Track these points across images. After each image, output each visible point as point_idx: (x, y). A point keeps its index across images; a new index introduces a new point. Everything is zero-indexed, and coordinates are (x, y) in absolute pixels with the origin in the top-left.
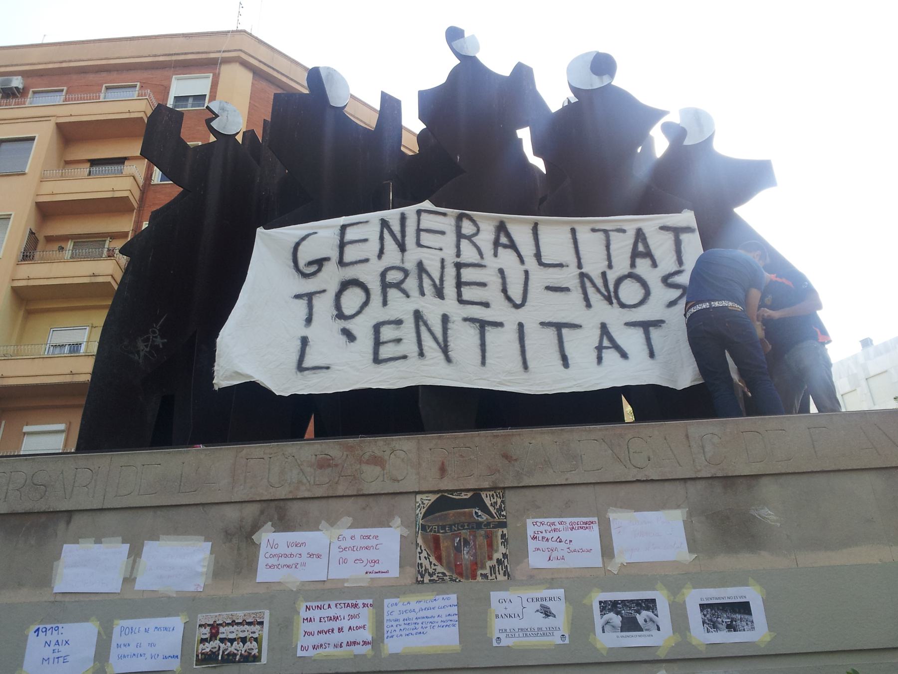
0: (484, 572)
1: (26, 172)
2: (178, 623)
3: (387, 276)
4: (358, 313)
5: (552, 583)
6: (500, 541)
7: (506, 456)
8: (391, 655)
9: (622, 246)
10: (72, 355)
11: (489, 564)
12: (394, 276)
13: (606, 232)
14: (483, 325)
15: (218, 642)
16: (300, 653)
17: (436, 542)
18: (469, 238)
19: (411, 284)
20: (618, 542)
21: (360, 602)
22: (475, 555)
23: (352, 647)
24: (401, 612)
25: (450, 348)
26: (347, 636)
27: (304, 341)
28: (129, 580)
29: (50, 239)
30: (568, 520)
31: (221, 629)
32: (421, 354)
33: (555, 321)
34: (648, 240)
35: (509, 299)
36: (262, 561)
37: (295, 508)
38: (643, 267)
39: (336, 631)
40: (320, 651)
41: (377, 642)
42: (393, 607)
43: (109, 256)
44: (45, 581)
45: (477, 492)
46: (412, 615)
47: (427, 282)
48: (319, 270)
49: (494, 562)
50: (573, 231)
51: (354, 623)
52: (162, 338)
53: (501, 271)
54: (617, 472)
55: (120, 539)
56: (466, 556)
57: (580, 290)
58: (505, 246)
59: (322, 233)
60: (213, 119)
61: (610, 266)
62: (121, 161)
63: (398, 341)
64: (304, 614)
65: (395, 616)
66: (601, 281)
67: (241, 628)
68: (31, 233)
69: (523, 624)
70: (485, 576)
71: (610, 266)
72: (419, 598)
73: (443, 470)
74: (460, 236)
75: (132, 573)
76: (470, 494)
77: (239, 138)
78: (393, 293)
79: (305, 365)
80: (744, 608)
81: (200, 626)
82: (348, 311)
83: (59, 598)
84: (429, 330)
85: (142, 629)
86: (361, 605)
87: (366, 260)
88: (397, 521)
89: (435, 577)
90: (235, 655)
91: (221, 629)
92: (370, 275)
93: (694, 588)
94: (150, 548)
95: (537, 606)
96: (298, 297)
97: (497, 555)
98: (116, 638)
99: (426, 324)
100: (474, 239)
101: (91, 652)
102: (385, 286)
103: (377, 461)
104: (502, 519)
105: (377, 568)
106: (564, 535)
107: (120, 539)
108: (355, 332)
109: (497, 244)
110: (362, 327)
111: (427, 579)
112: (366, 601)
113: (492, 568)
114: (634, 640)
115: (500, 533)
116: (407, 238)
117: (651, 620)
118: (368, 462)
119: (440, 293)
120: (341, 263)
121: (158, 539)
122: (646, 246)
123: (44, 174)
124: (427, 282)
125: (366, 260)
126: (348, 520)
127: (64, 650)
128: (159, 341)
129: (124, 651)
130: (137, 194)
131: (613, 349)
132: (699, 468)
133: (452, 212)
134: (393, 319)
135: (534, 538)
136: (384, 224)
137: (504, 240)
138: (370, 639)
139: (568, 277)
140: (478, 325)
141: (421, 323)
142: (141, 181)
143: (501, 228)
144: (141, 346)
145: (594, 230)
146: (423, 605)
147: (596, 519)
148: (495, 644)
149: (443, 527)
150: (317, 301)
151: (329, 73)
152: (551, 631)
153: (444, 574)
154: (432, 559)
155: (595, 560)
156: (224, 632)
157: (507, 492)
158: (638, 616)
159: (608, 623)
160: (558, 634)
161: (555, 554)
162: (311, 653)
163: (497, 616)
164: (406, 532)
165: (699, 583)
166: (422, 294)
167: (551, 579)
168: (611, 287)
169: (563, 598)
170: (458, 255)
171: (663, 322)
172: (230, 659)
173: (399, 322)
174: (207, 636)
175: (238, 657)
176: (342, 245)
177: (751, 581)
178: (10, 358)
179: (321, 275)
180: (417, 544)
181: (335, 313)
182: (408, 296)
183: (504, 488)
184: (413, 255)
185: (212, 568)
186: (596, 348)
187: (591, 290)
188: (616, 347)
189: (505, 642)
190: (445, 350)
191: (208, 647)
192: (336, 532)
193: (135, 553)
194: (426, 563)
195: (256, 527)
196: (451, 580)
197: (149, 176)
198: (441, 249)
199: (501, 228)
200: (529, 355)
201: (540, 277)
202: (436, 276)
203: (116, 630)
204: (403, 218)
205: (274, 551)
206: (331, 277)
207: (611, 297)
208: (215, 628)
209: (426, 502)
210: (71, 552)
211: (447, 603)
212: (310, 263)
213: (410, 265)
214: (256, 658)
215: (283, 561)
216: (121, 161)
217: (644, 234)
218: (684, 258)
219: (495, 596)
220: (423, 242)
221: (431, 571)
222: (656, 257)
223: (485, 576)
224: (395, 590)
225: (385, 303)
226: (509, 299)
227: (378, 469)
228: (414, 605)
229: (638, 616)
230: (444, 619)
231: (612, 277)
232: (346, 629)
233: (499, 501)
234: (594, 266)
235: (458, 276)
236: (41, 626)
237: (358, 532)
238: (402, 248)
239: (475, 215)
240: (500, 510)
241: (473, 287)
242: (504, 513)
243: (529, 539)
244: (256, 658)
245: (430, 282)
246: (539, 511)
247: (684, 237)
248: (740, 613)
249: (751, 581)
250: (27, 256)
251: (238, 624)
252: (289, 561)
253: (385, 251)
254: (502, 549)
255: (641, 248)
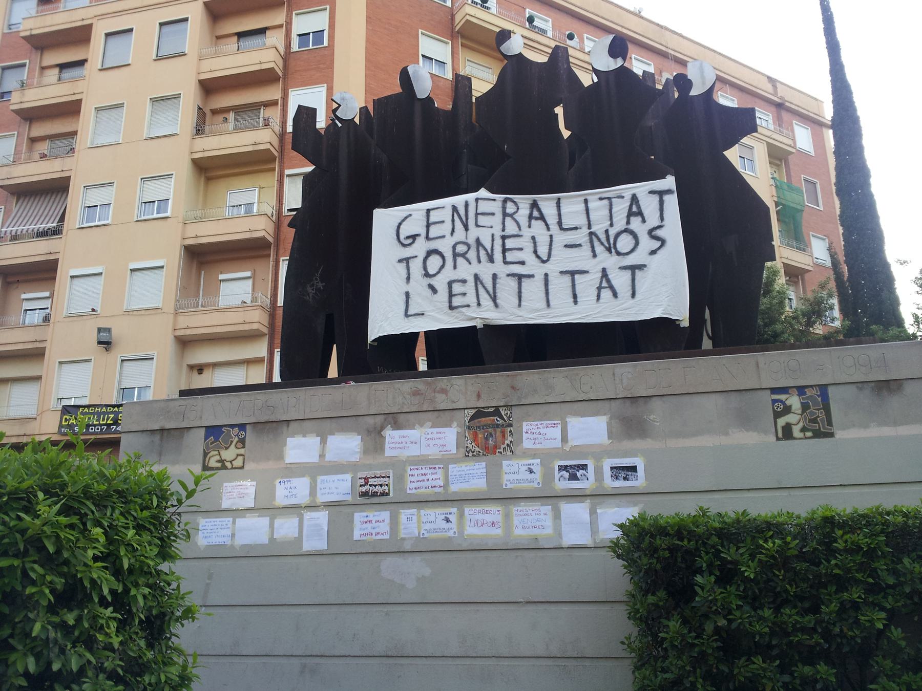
0: (499, 450)
1: (186, 52)
2: (348, 477)
3: (457, 248)
4: (438, 272)
5: (534, 456)
6: (509, 434)
7: (513, 388)
8: (453, 492)
9: (621, 208)
10: (249, 215)
11: (503, 446)
12: (461, 249)
13: (609, 199)
14: (520, 277)
15: (368, 486)
16: (408, 492)
17: (476, 435)
18: (511, 215)
19: (472, 255)
20: (571, 433)
21: (437, 466)
22: (496, 442)
23: (434, 489)
24: (458, 471)
25: (497, 298)
26: (430, 483)
27: (407, 295)
28: (322, 456)
29: (215, 112)
30: (545, 423)
31: (370, 480)
32: (479, 304)
33: (570, 269)
34: (640, 202)
35: (538, 257)
36: (387, 445)
37: (402, 418)
38: (636, 223)
39: (426, 480)
40: (418, 490)
41: (446, 486)
42: (454, 469)
43: (266, 125)
44: (280, 457)
45: (497, 408)
46: (462, 473)
47: (482, 253)
48: (413, 242)
49: (505, 445)
50: (586, 201)
51: (434, 477)
52: (322, 283)
53: (533, 238)
54: (573, 396)
55: (315, 434)
56: (491, 442)
57: (589, 244)
58: (537, 219)
59: (416, 215)
60: (337, 109)
61: (611, 225)
62: (262, 31)
63: (464, 294)
64: (409, 472)
65: (455, 473)
66: (605, 236)
67: (379, 479)
68: (200, 109)
69: (519, 477)
70: (501, 453)
71: (611, 225)
72: (467, 464)
73: (479, 396)
74: (505, 215)
75: (323, 452)
76: (493, 409)
77: (357, 120)
78: (460, 260)
79: (409, 313)
80: (634, 469)
81: (360, 478)
82: (431, 271)
83: (288, 466)
84: (484, 287)
85: (331, 480)
86: (437, 468)
87: (444, 237)
88: (455, 424)
89: (475, 453)
90: (377, 492)
91: (370, 480)
92: (445, 246)
93: (609, 458)
94: (331, 439)
95: (443, 517)
96: (400, 261)
97: (507, 442)
98: (319, 485)
99: (482, 283)
100: (515, 216)
101: (307, 492)
102: (455, 255)
103: (444, 391)
104: (510, 422)
105: (445, 449)
106: (543, 431)
107: (315, 434)
108: (436, 287)
109: (531, 217)
110: (440, 282)
111: (471, 454)
112: (440, 466)
113: (504, 449)
114: (575, 485)
115: (509, 430)
116: (469, 220)
117: (585, 475)
118: (439, 392)
119: (491, 259)
120: (427, 238)
121: (334, 435)
122: (639, 207)
123: (201, 53)
124: (482, 253)
125: (444, 237)
126: (429, 424)
127: (295, 492)
128: (320, 285)
129: (324, 491)
130: (280, 63)
131: (608, 289)
132: (618, 392)
133: (500, 197)
134: (460, 279)
135: (526, 433)
136: (455, 209)
137: (536, 214)
138: (442, 485)
139: (581, 236)
140: (517, 278)
141: (478, 283)
142: (282, 51)
143: (534, 205)
144: (309, 290)
145: (601, 199)
146: (468, 468)
147: (560, 422)
148: (504, 487)
149: (479, 427)
150: (412, 264)
151: (415, 70)
152: (533, 480)
153: (479, 452)
154: (473, 444)
155: (558, 444)
156: (371, 481)
157: (513, 407)
158: (577, 473)
159: (562, 476)
160: (536, 482)
161: (537, 441)
162: (414, 491)
163: (506, 473)
164: (459, 430)
165: (611, 455)
166: (479, 262)
167: (534, 454)
168: (612, 241)
169: (539, 464)
170: (503, 230)
171: (645, 266)
172: (375, 494)
173: (464, 281)
174: (363, 483)
175: (379, 494)
176: (428, 226)
177: (639, 455)
178: (200, 220)
179: (414, 245)
180: (466, 436)
181: (424, 272)
182: (470, 263)
183: (512, 406)
184: (474, 232)
185: (363, 448)
186: (597, 288)
187: (596, 243)
188: (611, 287)
189: (509, 486)
190: (494, 299)
191: (364, 489)
192: (424, 430)
193: (324, 442)
194: (470, 446)
195: (382, 428)
196: (483, 455)
197: (289, 43)
198: (492, 227)
199: (534, 205)
200: (550, 297)
201: (561, 238)
202: (489, 247)
203: (319, 481)
204: (467, 205)
205: (393, 441)
206: (420, 248)
207: (611, 248)
208: (366, 479)
209: (470, 413)
210: (292, 442)
211: (481, 467)
212: (408, 237)
213: (471, 241)
214: (388, 494)
215: (397, 445)
216: (262, 31)
217: (637, 198)
218: (665, 216)
219: (505, 463)
220: (479, 224)
221: (473, 450)
222: (645, 215)
223: (501, 453)
224: (455, 460)
225: (455, 267)
226: (538, 257)
227: (444, 395)
228: (464, 468)
229: (577, 473)
230: (479, 474)
231: (612, 232)
232: (430, 480)
233: (509, 412)
234: (599, 228)
235: (504, 244)
236: (282, 480)
237: (435, 430)
238: (466, 228)
239: (516, 198)
240: (509, 417)
241: (514, 251)
242: (511, 419)
243: (524, 433)
244: (388, 494)
245: (485, 252)
246: (527, 417)
247: (666, 198)
248: (631, 471)
249: (639, 455)
250: (199, 130)
251: (378, 477)
252: (400, 445)
253: (455, 230)
254: (510, 439)
255: (634, 209)
